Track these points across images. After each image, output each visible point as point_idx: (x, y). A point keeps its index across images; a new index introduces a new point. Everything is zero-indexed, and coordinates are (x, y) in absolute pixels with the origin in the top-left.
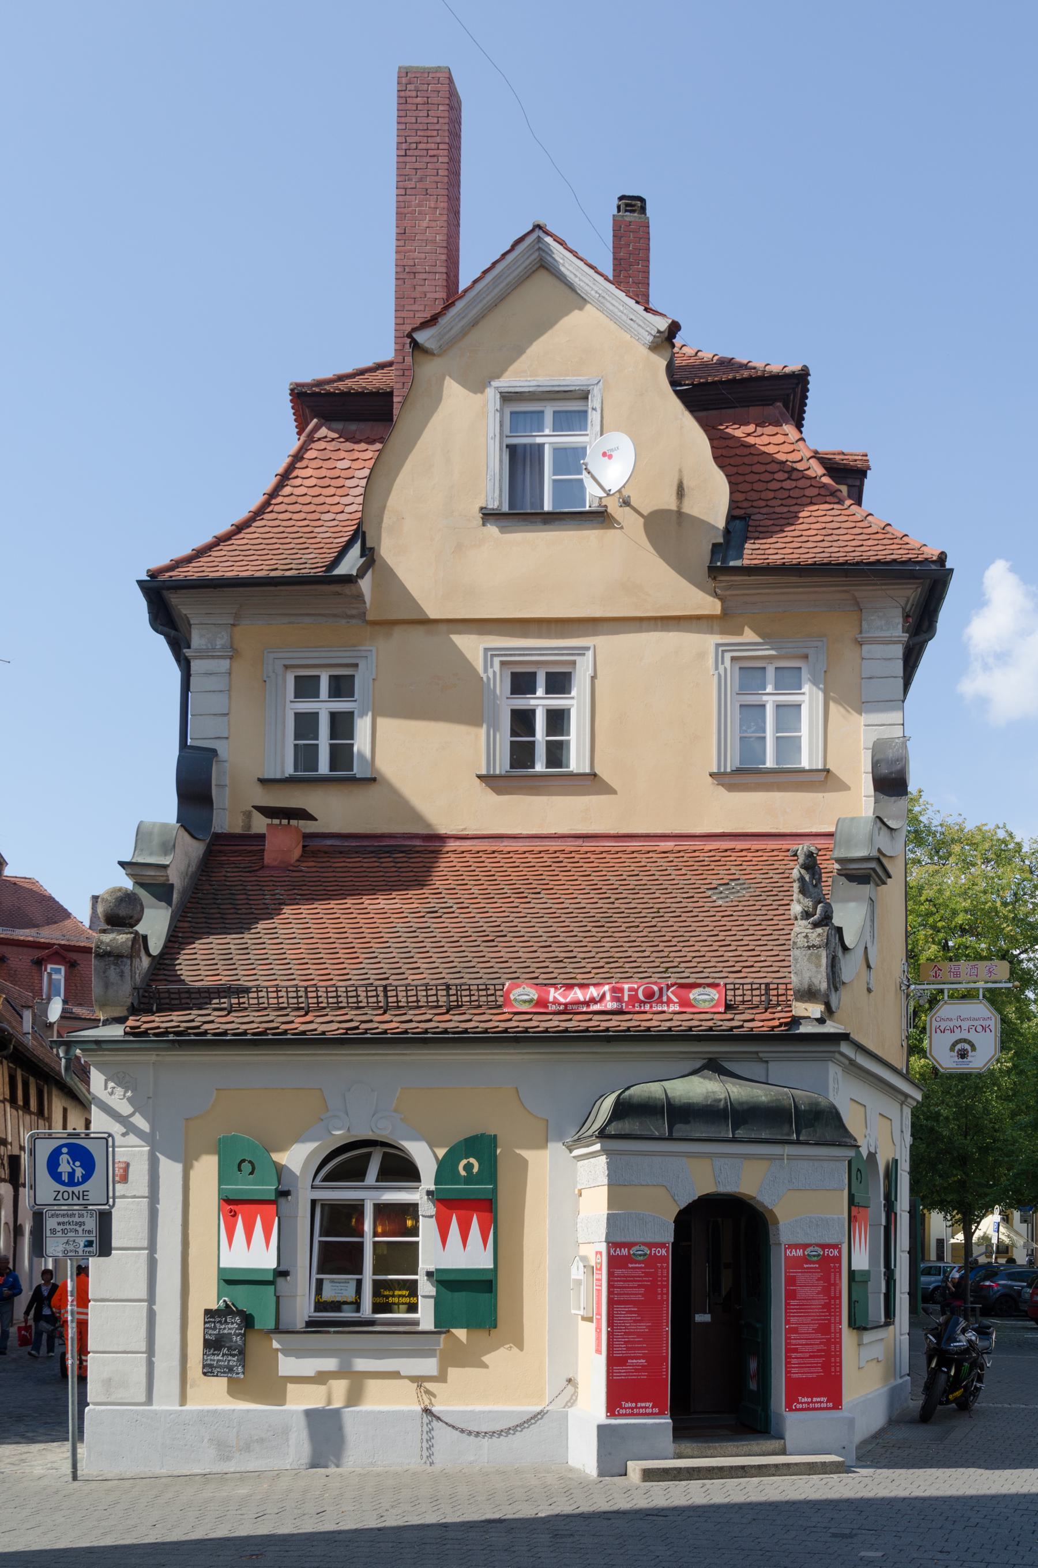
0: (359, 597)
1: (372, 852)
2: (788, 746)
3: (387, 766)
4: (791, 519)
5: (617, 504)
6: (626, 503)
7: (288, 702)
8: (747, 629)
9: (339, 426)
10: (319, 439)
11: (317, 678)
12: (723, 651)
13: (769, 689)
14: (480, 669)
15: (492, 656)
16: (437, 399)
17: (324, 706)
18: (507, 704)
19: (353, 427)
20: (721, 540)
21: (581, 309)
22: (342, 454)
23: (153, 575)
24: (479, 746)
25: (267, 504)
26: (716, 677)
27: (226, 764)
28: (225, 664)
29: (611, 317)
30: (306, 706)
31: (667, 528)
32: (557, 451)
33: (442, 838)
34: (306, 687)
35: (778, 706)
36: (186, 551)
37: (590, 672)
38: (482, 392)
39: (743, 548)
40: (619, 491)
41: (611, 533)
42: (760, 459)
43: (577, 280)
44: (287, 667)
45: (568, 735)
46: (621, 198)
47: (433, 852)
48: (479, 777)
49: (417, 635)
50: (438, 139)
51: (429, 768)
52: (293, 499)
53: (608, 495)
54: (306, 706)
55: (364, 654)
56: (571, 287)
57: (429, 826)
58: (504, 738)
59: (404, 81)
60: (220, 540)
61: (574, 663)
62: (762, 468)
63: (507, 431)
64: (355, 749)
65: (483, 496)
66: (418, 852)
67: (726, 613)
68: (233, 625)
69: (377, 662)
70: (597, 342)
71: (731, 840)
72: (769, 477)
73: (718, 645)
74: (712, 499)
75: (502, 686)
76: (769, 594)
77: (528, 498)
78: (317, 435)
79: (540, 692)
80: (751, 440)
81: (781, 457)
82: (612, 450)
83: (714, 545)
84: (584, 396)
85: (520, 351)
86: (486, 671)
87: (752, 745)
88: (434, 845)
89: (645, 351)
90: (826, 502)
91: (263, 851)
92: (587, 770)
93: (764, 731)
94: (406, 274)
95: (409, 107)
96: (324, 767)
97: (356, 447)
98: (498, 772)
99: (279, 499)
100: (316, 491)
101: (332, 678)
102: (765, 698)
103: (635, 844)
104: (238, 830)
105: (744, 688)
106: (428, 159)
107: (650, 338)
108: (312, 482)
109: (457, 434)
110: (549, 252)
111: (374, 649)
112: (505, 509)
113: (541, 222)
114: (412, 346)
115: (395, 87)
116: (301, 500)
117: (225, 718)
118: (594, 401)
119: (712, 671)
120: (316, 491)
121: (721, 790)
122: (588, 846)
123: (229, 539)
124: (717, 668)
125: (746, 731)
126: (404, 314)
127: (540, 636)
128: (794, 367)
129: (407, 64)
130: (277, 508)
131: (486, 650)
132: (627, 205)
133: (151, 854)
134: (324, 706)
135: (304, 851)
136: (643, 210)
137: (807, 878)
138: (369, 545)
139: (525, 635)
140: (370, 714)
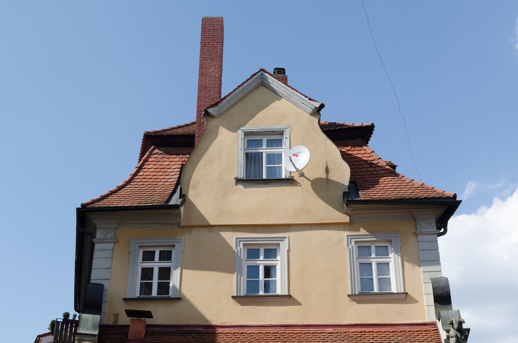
0: (179, 215)
1: (181, 333)
2: (384, 282)
3: (187, 292)
4: (377, 183)
5: (298, 176)
6: (302, 175)
7: (139, 263)
8: (361, 229)
9: (164, 149)
10: (155, 154)
11: (154, 252)
12: (351, 239)
13: (373, 256)
14: (234, 247)
15: (239, 241)
16: (216, 134)
17: (156, 265)
18: (245, 264)
19: (169, 149)
20: (347, 190)
21: (279, 100)
22: (165, 159)
23: (84, 206)
24: (230, 283)
25: (132, 178)
26: (348, 250)
27: (108, 291)
28: (111, 246)
29: (293, 103)
30: (148, 265)
31: (322, 186)
32: (269, 156)
33: (214, 327)
34: (149, 256)
35: (378, 264)
36: (98, 197)
37: (287, 248)
38: (236, 132)
39: (359, 194)
40: (301, 170)
41: (296, 187)
42: (355, 159)
43: (278, 89)
44: (140, 247)
45: (276, 277)
46: (275, 69)
47: (211, 333)
48: (233, 297)
49: (204, 233)
50: (218, 41)
51: (206, 293)
52: (144, 177)
53: (298, 171)
54: (148, 265)
55: (178, 241)
56: (275, 92)
57: (207, 321)
58: (244, 279)
59: (204, 21)
60: (112, 193)
61: (279, 244)
62: (357, 163)
63: (246, 147)
64: (171, 284)
65: (236, 173)
66: (204, 333)
67: (351, 222)
68: (116, 228)
69: (184, 245)
70: (285, 112)
71: (360, 328)
72: (361, 166)
73: (348, 236)
74: (343, 174)
75: (243, 255)
76: (372, 213)
77: (256, 173)
78: (154, 152)
79: (262, 258)
80: (349, 152)
81: (364, 159)
82: (298, 153)
83: (344, 193)
84: (282, 133)
85: (253, 116)
86: (236, 248)
87: (367, 282)
88: (211, 330)
89: (309, 116)
90: (390, 176)
91: (128, 333)
92: (287, 294)
93: (372, 275)
94: (202, 88)
95: (206, 30)
96: (154, 293)
97: (171, 156)
98: (242, 295)
99: (138, 177)
100: (154, 173)
101: (160, 252)
102: (371, 260)
103: (312, 330)
104: (111, 323)
105: (360, 256)
106: (213, 48)
107: (311, 110)
108: (152, 170)
109: (224, 150)
110: (266, 80)
111: (183, 238)
112: (245, 178)
113: (263, 68)
114: (205, 114)
115: (201, 24)
116: (147, 177)
117: (109, 270)
118: (286, 135)
119: (346, 247)
120: (154, 173)
121: (354, 303)
122: (289, 330)
123: (116, 192)
124: (348, 246)
125: (362, 276)
126: (202, 103)
127: (267, 233)
128: (369, 123)
129: (206, 16)
130: (136, 180)
131: (237, 238)
132: (278, 71)
133: (88, 330)
134: (156, 265)
135: (146, 333)
136: (284, 73)
137: (459, 335)
138: (183, 193)
139: (255, 232)
140: (180, 268)
